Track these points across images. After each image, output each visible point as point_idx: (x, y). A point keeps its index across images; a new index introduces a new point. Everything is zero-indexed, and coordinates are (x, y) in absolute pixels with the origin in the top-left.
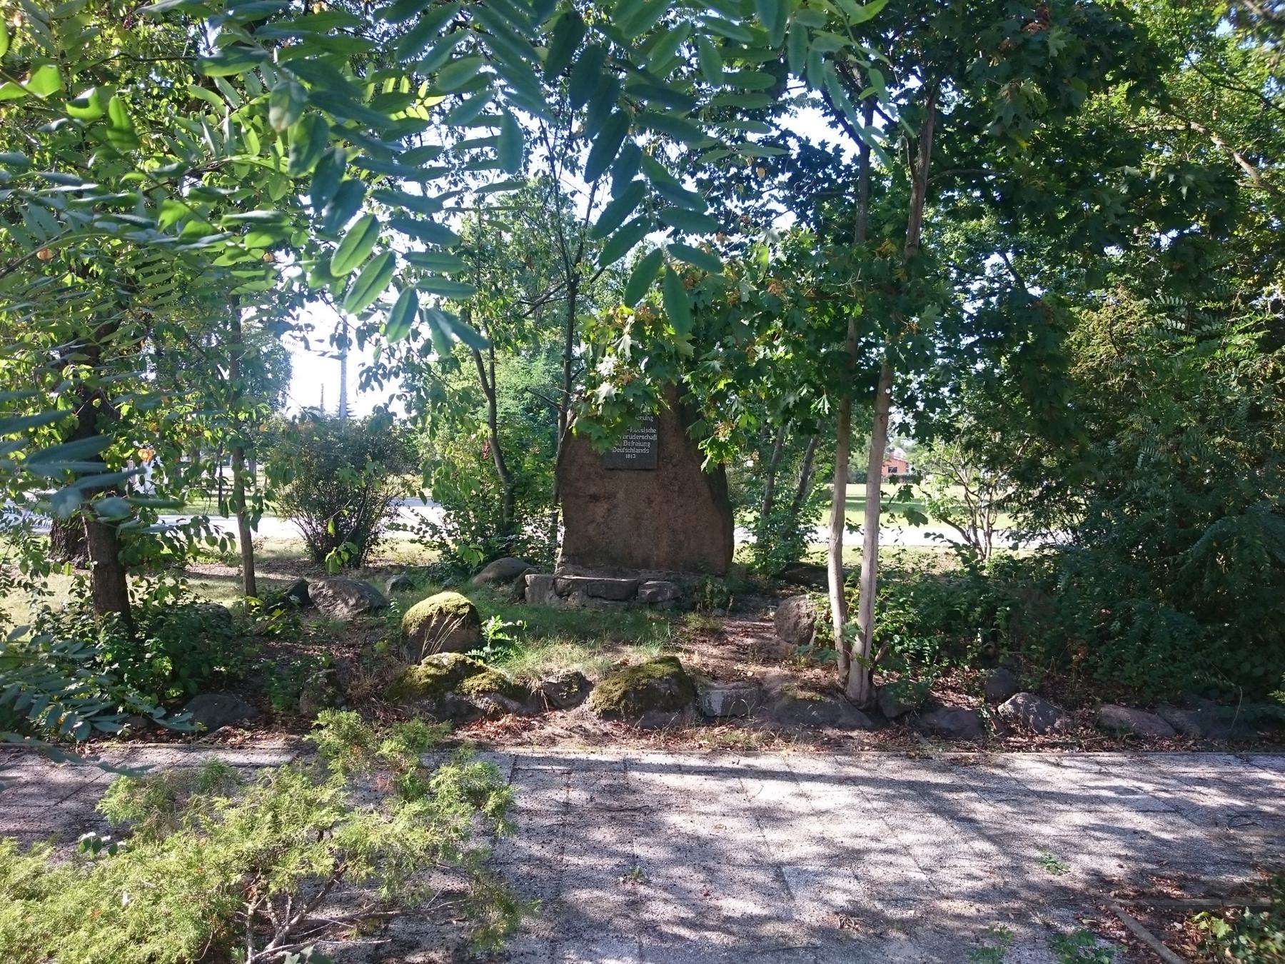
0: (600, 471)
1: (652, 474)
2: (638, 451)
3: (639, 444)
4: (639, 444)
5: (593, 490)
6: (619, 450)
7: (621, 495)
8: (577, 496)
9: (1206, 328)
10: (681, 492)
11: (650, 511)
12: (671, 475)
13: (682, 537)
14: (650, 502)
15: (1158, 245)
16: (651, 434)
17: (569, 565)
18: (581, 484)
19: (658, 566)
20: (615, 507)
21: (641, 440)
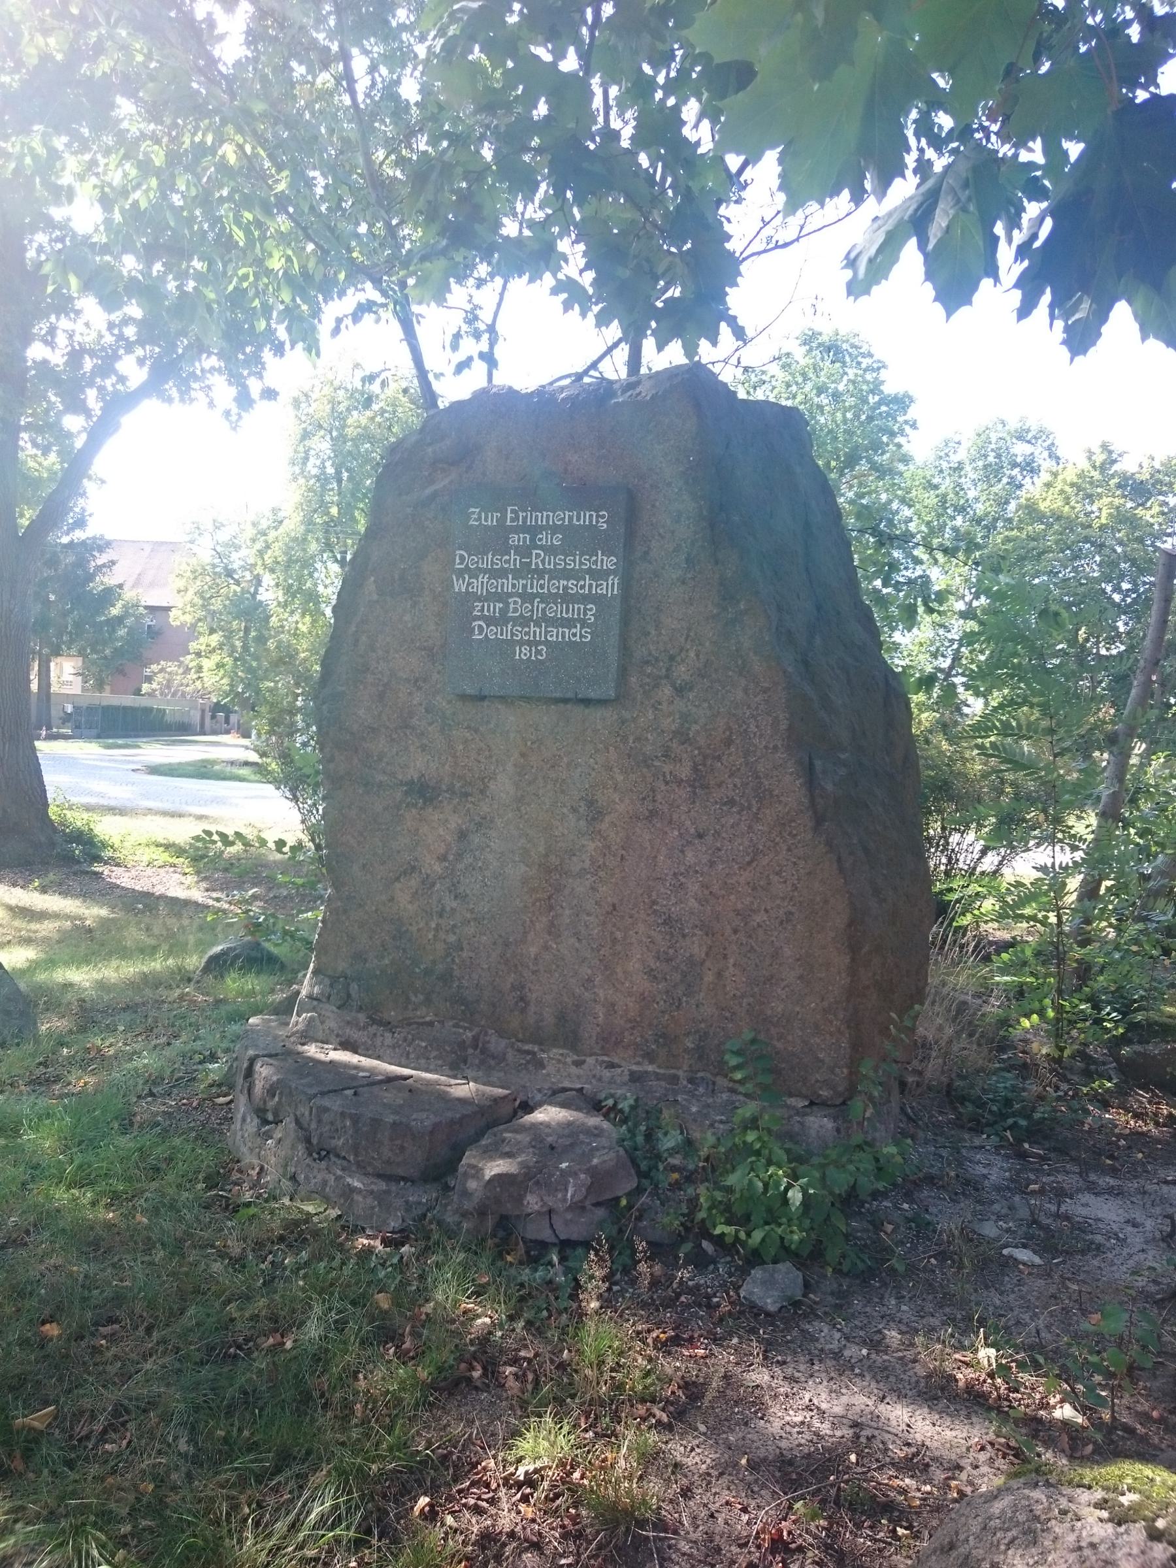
2: (555, 635)
3: (556, 610)
4: (556, 610)
5: (418, 765)
6: (492, 632)
7: (503, 786)
13: (696, 947)
14: (595, 813)
16: (599, 575)
17: (329, 1009)
21: (567, 598)
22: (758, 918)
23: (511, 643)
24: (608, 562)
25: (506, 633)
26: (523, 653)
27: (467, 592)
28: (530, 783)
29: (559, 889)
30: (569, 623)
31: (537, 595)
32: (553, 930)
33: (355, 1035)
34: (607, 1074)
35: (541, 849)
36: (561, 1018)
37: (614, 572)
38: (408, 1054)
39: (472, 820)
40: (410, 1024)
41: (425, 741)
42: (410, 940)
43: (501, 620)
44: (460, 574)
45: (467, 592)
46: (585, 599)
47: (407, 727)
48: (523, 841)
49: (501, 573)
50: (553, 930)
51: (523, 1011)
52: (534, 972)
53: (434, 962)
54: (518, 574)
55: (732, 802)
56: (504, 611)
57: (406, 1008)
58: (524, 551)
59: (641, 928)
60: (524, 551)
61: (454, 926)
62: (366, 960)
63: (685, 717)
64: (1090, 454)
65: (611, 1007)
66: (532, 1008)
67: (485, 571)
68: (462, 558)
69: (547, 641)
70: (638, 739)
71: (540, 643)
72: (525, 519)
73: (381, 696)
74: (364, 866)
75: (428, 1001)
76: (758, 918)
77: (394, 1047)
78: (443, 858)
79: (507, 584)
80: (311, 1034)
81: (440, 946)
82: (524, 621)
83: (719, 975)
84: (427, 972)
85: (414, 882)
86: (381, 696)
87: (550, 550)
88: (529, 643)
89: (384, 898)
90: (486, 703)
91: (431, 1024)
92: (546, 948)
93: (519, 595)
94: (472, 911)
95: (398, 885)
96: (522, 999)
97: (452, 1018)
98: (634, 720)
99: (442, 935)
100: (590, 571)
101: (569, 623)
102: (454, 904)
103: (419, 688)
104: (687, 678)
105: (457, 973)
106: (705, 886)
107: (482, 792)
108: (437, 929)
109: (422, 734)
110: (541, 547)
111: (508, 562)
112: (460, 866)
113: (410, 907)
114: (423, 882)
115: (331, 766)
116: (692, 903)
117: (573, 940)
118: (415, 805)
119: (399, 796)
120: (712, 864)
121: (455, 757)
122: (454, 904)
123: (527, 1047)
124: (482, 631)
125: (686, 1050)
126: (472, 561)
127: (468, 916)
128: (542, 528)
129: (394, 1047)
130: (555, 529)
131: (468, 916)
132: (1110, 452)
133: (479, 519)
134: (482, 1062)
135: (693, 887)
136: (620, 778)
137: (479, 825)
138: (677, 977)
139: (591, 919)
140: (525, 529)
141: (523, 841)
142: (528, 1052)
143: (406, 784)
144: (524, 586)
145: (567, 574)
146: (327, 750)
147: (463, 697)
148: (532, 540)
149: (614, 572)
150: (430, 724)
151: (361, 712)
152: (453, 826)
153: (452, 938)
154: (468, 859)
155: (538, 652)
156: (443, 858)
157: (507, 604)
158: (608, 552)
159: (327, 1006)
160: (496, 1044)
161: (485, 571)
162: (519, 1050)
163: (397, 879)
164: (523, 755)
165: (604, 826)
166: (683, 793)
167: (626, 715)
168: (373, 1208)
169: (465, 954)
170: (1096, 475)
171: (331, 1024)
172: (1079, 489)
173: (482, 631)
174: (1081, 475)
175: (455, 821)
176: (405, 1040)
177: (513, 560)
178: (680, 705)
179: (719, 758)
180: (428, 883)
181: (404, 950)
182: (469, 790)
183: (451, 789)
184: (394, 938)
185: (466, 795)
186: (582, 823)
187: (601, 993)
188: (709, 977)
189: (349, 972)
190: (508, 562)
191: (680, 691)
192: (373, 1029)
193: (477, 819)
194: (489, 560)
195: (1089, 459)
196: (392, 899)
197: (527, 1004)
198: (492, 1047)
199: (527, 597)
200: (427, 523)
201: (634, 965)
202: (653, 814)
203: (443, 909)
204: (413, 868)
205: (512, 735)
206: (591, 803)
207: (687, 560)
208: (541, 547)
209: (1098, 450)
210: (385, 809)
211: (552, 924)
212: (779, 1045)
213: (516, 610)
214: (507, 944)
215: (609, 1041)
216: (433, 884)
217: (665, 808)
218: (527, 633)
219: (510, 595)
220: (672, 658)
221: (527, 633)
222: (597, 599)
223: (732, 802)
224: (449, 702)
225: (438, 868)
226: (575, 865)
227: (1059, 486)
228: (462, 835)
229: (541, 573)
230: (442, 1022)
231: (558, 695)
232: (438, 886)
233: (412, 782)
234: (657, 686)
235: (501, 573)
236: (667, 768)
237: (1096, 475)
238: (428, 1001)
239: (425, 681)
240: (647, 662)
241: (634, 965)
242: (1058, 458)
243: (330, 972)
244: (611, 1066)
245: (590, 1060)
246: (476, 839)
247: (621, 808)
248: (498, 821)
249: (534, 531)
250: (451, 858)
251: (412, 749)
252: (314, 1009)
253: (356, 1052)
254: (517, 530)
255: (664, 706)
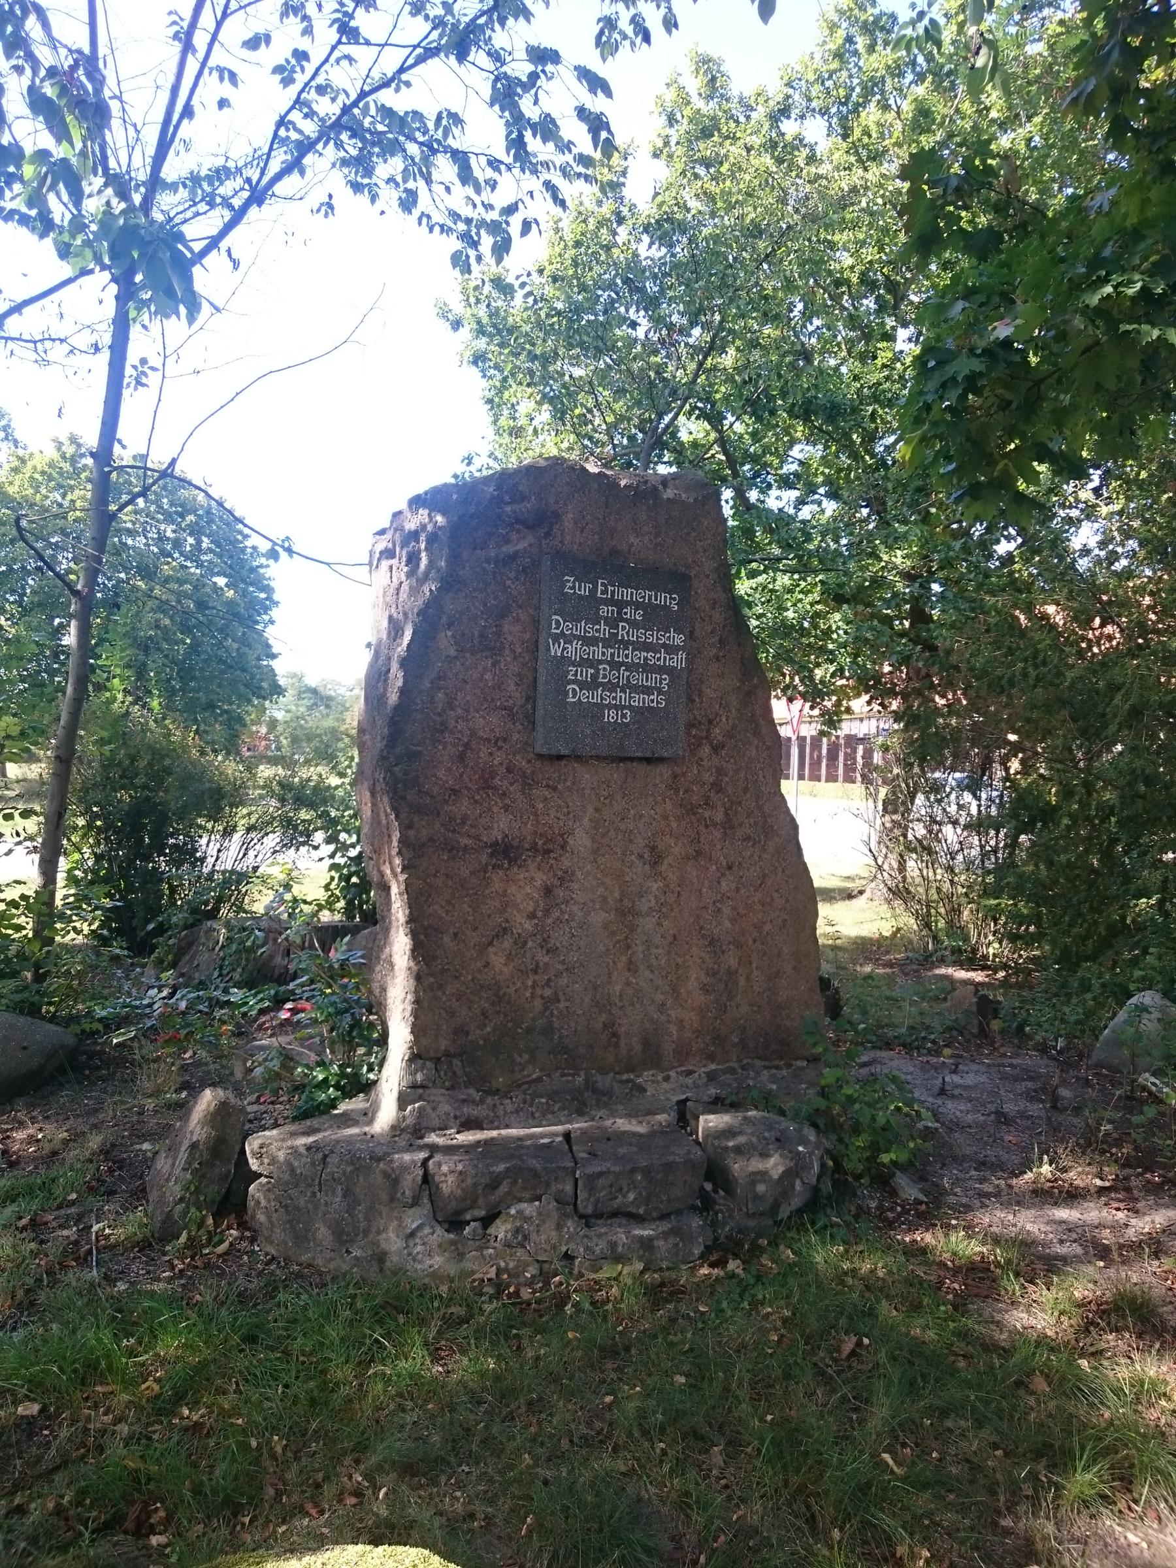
0: (520, 761)
1: (664, 771)
2: (638, 700)
3: (639, 679)
4: (639, 679)
5: (502, 826)
6: (585, 696)
7: (580, 840)
8: (451, 848)
9: (758, 713)
10: (728, 825)
11: (655, 886)
12: (708, 777)
13: (731, 959)
14: (656, 857)
15: (354, 1506)
16: (671, 649)
17: (437, 1093)
18: (463, 806)
19: (683, 1053)
20: (566, 877)
21: (647, 668)
22: (767, 928)
23: (601, 707)
24: (678, 640)
25: (596, 696)
26: (610, 716)
27: (562, 656)
28: (603, 836)
29: (632, 928)
30: (648, 691)
31: (622, 664)
32: (631, 967)
33: (468, 1110)
34: (689, 1081)
35: (617, 895)
36: (646, 1043)
37: (683, 648)
38: (532, 1114)
39: (555, 875)
40: (519, 1086)
41: (507, 801)
42: (509, 1003)
43: (593, 685)
44: (556, 639)
45: (562, 656)
46: (661, 670)
47: (489, 787)
48: (601, 889)
49: (591, 642)
50: (631, 967)
51: (617, 1045)
52: (621, 1008)
53: (534, 1019)
54: (607, 643)
55: (748, 838)
56: (595, 677)
57: (513, 1071)
58: (613, 623)
59: (695, 950)
60: (613, 623)
61: (549, 980)
62: (467, 1033)
63: (720, 771)
64: (59, 446)
65: (680, 1023)
66: (623, 1041)
67: (579, 638)
68: (558, 623)
69: (630, 707)
70: (686, 791)
71: (624, 707)
72: (613, 592)
73: (462, 757)
74: (455, 935)
75: (533, 1059)
76: (767, 928)
77: (517, 1112)
78: (532, 916)
79: (598, 652)
80: (425, 1124)
81: (538, 1003)
82: (612, 687)
83: (748, 979)
84: (529, 1030)
85: (507, 943)
86: (462, 757)
87: (633, 624)
88: (616, 707)
89: (479, 964)
90: (563, 763)
91: (539, 1080)
92: (628, 984)
93: (608, 663)
94: (563, 962)
95: (491, 950)
96: (614, 1035)
97: (557, 1068)
98: (684, 774)
99: (539, 991)
100: (664, 645)
101: (648, 691)
102: (546, 959)
103: (500, 748)
104: (720, 738)
105: (556, 1025)
106: (734, 908)
107: (563, 847)
108: (533, 987)
109: (504, 794)
110: (626, 621)
111: (598, 631)
112: (549, 921)
113: (505, 969)
114: (515, 943)
115: (411, 833)
116: (727, 924)
117: (647, 973)
118: (500, 867)
119: (484, 858)
120: (738, 889)
121: (536, 815)
122: (546, 959)
123: (625, 1077)
124: (575, 695)
125: (734, 1045)
126: (567, 628)
127: (561, 967)
128: (628, 603)
129: (517, 1112)
130: (637, 606)
131: (561, 967)
132: (79, 446)
133: (573, 588)
134: (598, 1101)
135: (726, 910)
136: (674, 825)
137: (561, 879)
138: (722, 987)
139: (660, 951)
140: (612, 602)
141: (601, 889)
142: (628, 1081)
143: (492, 845)
144: (612, 655)
145: (647, 647)
146: (403, 815)
147: (540, 757)
148: (619, 613)
149: (683, 648)
150: (512, 784)
151: (441, 774)
152: (538, 883)
153: (548, 992)
154: (556, 914)
155: (624, 716)
156: (532, 916)
157: (598, 670)
158: (678, 631)
159: (435, 1091)
160: (603, 1081)
161: (579, 638)
162: (621, 1082)
163: (490, 944)
164: (597, 810)
165: (664, 868)
166: (717, 834)
167: (678, 770)
168: (676, 1245)
169: (562, 1005)
170: (66, 466)
171: (445, 1108)
172: (50, 478)
173: (575, 695)
174: (51, 465)
175: (540, 878)
176: (525, 1102)
177: (604, 630)
178: (716, 760)
179: (740, 803)
180: (521, 942)
181: (506, 1015)
182: (551, 846)
183: (534, 848)
184: (493, 1004)
185: (549, 851)
186: (647, 867)
187: (672, 1013)
188: (742, 982)
189: (452, 1050)
190: (598, 631)
191: (716, 749)
192: (489, 1100)
193: (560, 873)
194: (582, 628)
195: (59, 449)
196: (487, 965)
197: (618, 1038)
198: (600, 1085)
199: (616, 666)
200: (508, 583)
201: (693, 984)
202: (699, 853)
203: (537, 966)
204: (505, 929)
205: (587, 792)
206: (653, 849)
207: (721, 641)
208: (626, 621)
209: (67, 443)
210: (472, 873)
211: (630, 962)
212: (787, 1023)
213: (605, 677)
214: (595, 988)
215: (683, 1053)
216: (525, 943)
217: (706, 847)
218: (615, 698)
219: (600, 662)
220: (710, 722)
221: (615, 698)
222: (669, 670)
223: (748, 838)
224: (529, 762)
225: (528, 926)
226: (643, 906)
227: (28, 470)
228: (548, 891)
229: (626, 644)
230: (549, 1075)
231: (639, 755)
232: (530, 944)
233: (495, 844)
234: (700, 745)
235: (591, 642)
236: (707, 814)
237: (66, 466)
238: (533, 1059)
239: (505, 740)
240: (693, 726)
241: (693, 984)
242: (16, 442)
243: (432, 1055)
244: (689, 1073)
245: (672, 1074)
246: (560, 893)
247: (676, 850)
248: (579, 874)
249: (621, 605)
250: (540, 914)
251: (495, 810)
252: (420, 1098)
253: (482, 1129)
254: (607, 602)
255: (705, 763)
